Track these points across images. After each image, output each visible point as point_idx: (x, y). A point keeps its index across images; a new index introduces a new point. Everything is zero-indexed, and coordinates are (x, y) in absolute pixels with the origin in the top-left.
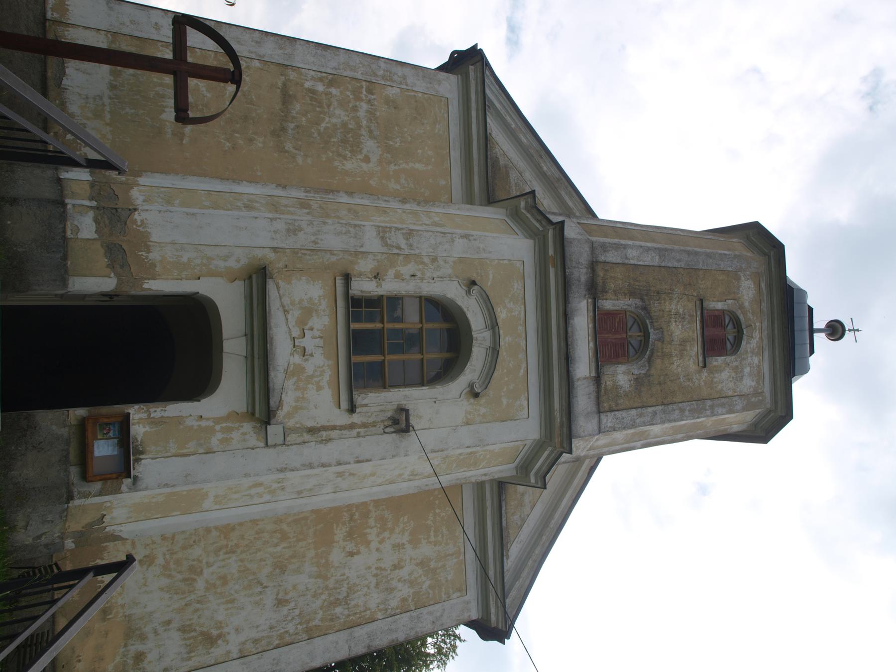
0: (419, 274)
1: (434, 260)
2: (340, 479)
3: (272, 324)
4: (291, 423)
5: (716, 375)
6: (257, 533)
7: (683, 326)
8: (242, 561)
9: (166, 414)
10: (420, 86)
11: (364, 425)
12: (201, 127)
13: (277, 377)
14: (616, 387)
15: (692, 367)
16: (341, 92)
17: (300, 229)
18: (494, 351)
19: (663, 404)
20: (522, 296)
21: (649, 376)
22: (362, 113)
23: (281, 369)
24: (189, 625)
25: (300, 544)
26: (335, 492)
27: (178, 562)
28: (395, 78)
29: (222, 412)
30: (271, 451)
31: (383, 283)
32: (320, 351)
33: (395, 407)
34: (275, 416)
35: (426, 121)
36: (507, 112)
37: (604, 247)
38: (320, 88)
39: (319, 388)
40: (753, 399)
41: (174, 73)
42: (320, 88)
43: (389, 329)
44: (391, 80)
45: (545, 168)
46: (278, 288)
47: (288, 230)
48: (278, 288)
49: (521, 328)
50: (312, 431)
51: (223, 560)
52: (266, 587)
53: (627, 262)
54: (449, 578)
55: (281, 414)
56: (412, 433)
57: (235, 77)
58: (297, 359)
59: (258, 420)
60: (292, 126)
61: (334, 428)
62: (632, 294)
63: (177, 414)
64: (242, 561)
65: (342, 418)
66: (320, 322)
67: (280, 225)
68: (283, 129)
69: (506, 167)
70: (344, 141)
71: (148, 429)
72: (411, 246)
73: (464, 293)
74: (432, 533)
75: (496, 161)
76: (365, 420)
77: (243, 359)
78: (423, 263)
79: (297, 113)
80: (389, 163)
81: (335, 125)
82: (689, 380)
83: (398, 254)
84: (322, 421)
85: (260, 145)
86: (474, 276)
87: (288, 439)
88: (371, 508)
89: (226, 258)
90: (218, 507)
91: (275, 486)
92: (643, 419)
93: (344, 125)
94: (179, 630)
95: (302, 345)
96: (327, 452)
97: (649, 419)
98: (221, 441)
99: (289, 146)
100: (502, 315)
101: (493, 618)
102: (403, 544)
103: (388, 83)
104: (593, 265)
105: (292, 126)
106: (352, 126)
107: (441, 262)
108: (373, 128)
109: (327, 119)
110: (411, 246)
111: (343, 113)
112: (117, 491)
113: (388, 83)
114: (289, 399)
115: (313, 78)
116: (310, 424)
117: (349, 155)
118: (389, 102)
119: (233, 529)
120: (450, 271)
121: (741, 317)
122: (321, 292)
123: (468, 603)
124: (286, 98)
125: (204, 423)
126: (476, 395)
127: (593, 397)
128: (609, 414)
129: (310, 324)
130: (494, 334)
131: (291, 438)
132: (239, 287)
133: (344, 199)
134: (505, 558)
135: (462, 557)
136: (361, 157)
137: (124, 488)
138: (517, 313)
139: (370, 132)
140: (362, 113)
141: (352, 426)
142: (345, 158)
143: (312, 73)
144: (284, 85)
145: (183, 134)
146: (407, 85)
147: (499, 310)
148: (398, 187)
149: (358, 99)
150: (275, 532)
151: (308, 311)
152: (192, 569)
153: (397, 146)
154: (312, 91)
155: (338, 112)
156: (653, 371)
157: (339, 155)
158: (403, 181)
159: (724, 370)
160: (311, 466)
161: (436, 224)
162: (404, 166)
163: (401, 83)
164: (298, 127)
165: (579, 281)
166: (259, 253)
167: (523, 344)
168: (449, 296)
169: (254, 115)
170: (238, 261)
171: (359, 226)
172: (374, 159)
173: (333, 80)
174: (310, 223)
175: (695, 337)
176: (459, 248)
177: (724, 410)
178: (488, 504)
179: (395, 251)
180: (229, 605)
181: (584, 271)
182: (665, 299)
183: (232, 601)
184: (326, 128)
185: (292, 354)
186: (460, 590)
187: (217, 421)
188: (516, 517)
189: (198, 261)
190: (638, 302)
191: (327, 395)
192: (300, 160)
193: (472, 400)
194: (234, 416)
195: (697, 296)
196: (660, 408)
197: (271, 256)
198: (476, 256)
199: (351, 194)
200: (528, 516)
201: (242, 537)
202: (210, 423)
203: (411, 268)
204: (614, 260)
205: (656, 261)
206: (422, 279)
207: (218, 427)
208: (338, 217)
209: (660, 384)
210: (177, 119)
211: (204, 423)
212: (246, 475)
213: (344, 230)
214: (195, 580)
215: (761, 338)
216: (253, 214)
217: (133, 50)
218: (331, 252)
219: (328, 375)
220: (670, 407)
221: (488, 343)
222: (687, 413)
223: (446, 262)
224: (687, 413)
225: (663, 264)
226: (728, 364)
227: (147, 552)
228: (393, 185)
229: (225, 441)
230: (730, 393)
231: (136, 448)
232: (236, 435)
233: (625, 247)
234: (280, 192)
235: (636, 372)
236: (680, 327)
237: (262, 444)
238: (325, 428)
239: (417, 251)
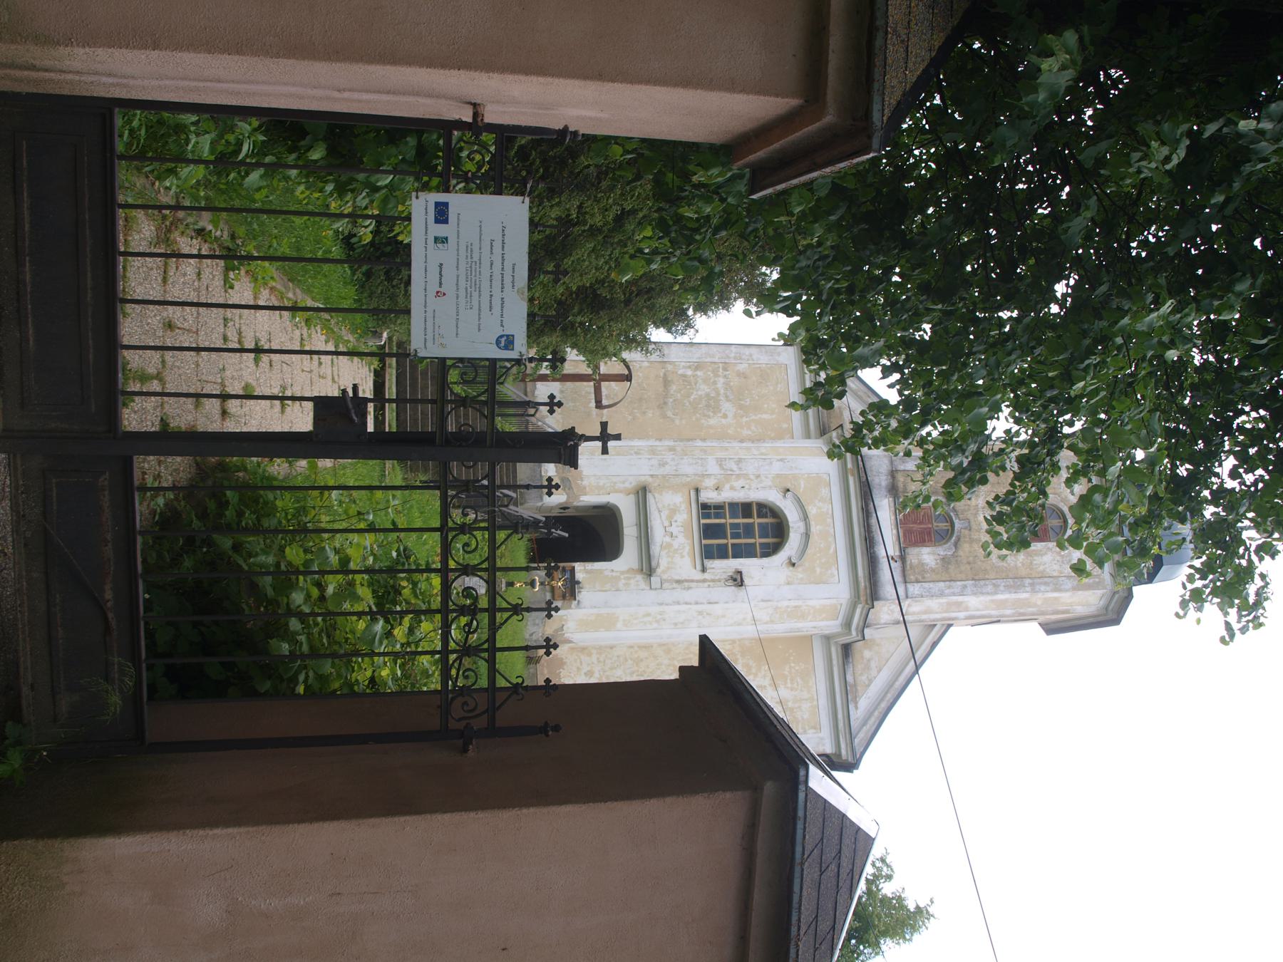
0: (747, 486)
3: (652, 519)
4: (665, 577)
5: (1035, 558)
6: (658, 665)
10: (763, 359)
11: (713, 581)
12: (613, 408)
13: (655, 549)
14: (922, 564)
17: (667, 463)
18: (807, 535)
19: (973, 579)
22: (720, 385)
23: (658, 544)
28: (743, 357)
29: (625, 568)
30: (653, 592)
31: (722, 493)
34: (655, 572)
38: (689, 373)
39: (682, 557)
42: (689, 373)
44: (741, 359)
47: (660, 464)
49: (830, 520)
50: (678, 582)
54: (805, 717)
55: (659, 571)
57: (628, 378)
58: (668, 539)
59: (645, 574)
60: (671, 400)
61: (692, 581)
63: (599, 568)
66: (682, 517)
67: (654, 462)
68: (665, 403)
70: (708, 406)
72: (740, 469)
73: (782, 497)
74: (789, 681)
76: (713, 577)
78: (749, 479)
80: (742, 417)
81: (701, 396)
84: (684, 577)
85: (651, 415)
86: (789, 486)
89: (624, 482)
91: (659, 617)
92: (952, 590)
93: (707, 395)
99: (669, 414)
100: (812, 511)
101: (844, 752)
102: (765, 686)
105: (671, 400)
107: (763, 478)
110: (740, 469)
111: (706, 387)
112: (570, 607)
115: (684, 367)
116: (677, 578)
117: (712, 414)
119: (642, 660)
122: (681, 499)
123: (822, 739)
124: (666, 382)
125: (614, 574)
126: (794, 565)
128: (915, 584)
129: (675, 518)
131: (665, 585)
132: (632, 498)
133: (699, 443)
134: (851, 706)
135: (815, 703)
136: (721, 415)
137: (573, 606)
139: (727, 397)
140: (720, 385)
141: (704, 581)
142: (709, 417)
143: (683, 364)
144: (665, 374)
145: (602, 414)
148: (750, 433)
150: (669, 665)
151: (673, 511)
153: (748, 404)
154: (684, 376)
155: (703, 387)
156: (960, 553)
157: (705, 415)
158: (753, 428)
159: (1046, 553)
160: (678, 603)
161: (762, 454)
162: (753, 417)
163: (748, 360)
164: (675, 400)
166: (643, 479)
169: (646, 396)
170: (631, 483)
171: (705, 459)
172: (730, 415)
174: (673, 459)
176: (777, 468)
177: (1048, 588)
178: (835, 662)
179: (731, 473)
181: (884, 478)
184: (695, 399)
185: (664, 536)
186: (815, 728)
187: (622, 573)
188: (864, 678)
189: (609, 485)
191: (687, 561)
192: (677, 422)
194: (631, 570)
196: (971, 582)
197: (650, 480)
199: (704, 440)
200: (875, 678)
201: (648, 667)
202: (618, 574)
203: (741, 482)
206: (749, 489)
207: (622, 577)
208: (693, 455)
209: (969, 563)
210: (597, 407)
211: (614, 574)
212: (640, 605)
213: (694, 462)
216: (640, 457)
218: (687, 476)
219: (687, 548)
220: (982, 583)
221: (802, 530)
222: (1002, 588)
223: (767, 478)
224: (1002, 588)
227: (589, 668)
228: (745, 432)
229: (626, 585)
230: (1055, 574)
232: (632, 581)
234: (658, 443)
235: (942, 553)
239: (745, 472)
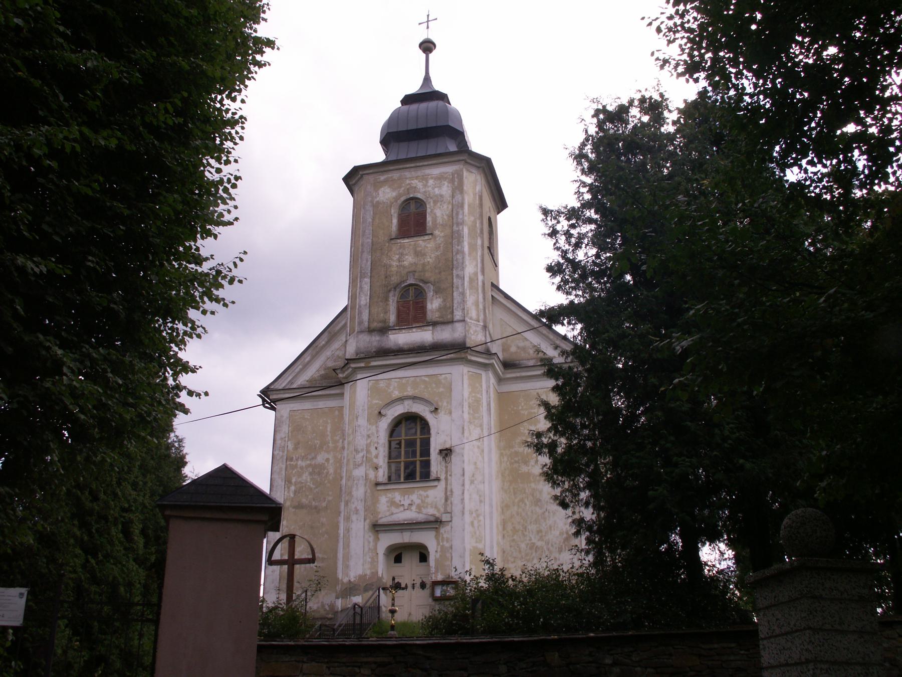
0: (376, 445)
1: (369, 436)
2: (475, 482)
4: (442, 510)
5: (438, 222)
7: (406, 255)
8: (531, 523)
9: (434, 566)
11: (446, 472)
13: (421, 517)
15: (431, 245)
16: (294, 476)
18: (414, 398)
19: (452, 270)
20: (387, 381)
21: (435, 282)
24: (559, 548)
25: (527, 491)
26: (484, 483)
27: (527, 555)
28: (283, 444)
32: (410, 496)
33: (439, 456)
35: (304, 425)
36: (293, 371)
37: (361, 323)
38: (293, 488)
39: (427, 496)
40: (456, 183)
41: (293, 565)
42: (293, 488)
43: (405, 459)
44: (284, 447)
45: (323, 343)
46: (382, 518)
47: (357, 514)
48: (382, 518)
50: (446, 499)
51: (529, 532)
52: (546, 510)
53: (368, 305)
55: (438, 515)
56: (452, 448)
58: (414, 508)
59: (439, 526)
60: (314, 503)
61: (446, 489)
62: (386, 299)
64: (531, 523)
65: (442, 484)
66: (397, 497)
68: (316, 507)
69: (325, 369)
70: (319, 474)
71: (439, 574)
72: (362, 450)
73: (385, 418)
74: (533, 411)
75: (324, 377)
76: (444, 472)
77: (412, 534)
78: (370, 443)
79: (307, 500)
80: (328, 446)
81: (311, 479)
82: (440, 247)
83: (366, 457)
84: (442, 495)
86: (377, 412)
87: (449, 511)
88: (513, 451)
89: (369, 542)
90: (483, 542)
93: (311, 474)
94: (560, 554)
95: (407, 505)
96: (457, 492)
97: (460, 281)
98: (447, 542)
99: (324, 504)
100: (396, 394)
103: (286, 448)
104: (370, 331)
105: (314, 503)
106: (310, 470)
107: (370, 432)
108: (311, 457)
109: (308, 484)
110: (362, 450)
111: (304, 475)
113: (286, 448)
114: (431, 511)
115: (288, 492)
116: (443, 501)
117: (326, 471)
118: (296, 448)
120: (374, 427)
121: (403, 199)
126: (436, 409)
127: (443, 327)
128: (455, 314)
129: (398, 502)
130: (405, 399)
132: (382, 536)
138: (396, 384)
139: (313, 458)
141: (446, 479)
142: (327, 473)
146: (285, 437)
147: (394, 396)
149: (296, 466)
151: (392, 503)
152: (531, 548)
154: (295, 492)
155: (304, 478)
156: (432, 279)
160: (463, 500)
162: (329, 438)
163: (285, 441)
164: (314, 500)
165: (379, 341)
166: (367, 527)
167: (412, 379)
168: (386, 427)
170: (371, 537)
173: (288, 481)
175: (413, 243)
177: (461, 212)
179: (365, 459)
180: (553, 528)
182: (390, 271)
183: (550, 527)
184: (313, 484)
185: (411, 510)
187: (438, 544)
189: (370, 554)
190: (391, 294)
191: (431, 493)
192: (330, 498)
193: (439, 411)
194: (437, 537)
195: (388, 242)
196: (454, 271)
197: (368, 521)
198: (366, 412)
200: (531, 343)
201: (519, 523)
202: (439, 547)
203: (373, 449)
204: (367, 315)
205: (367, 280)
206: (378, 443)
207: (441, 544)
209: (440, 273)
211: (439, 550)
214: (537, 547)
215: (417, 178)
217: (285, 581)
218: (366, 492)
221: (410, 402)
222: (459, 248)
224: (459, 248)
225: (369, 274)
226: (431, 212)
230: (450, 207)
231: (447, 578)
232: (445, 536)
233: (360, 306)
234: (342, 515)
235: (432, 293)
236: (407, 257)
237: (450, 523)
238: (446, 493)
239: (365, 446)
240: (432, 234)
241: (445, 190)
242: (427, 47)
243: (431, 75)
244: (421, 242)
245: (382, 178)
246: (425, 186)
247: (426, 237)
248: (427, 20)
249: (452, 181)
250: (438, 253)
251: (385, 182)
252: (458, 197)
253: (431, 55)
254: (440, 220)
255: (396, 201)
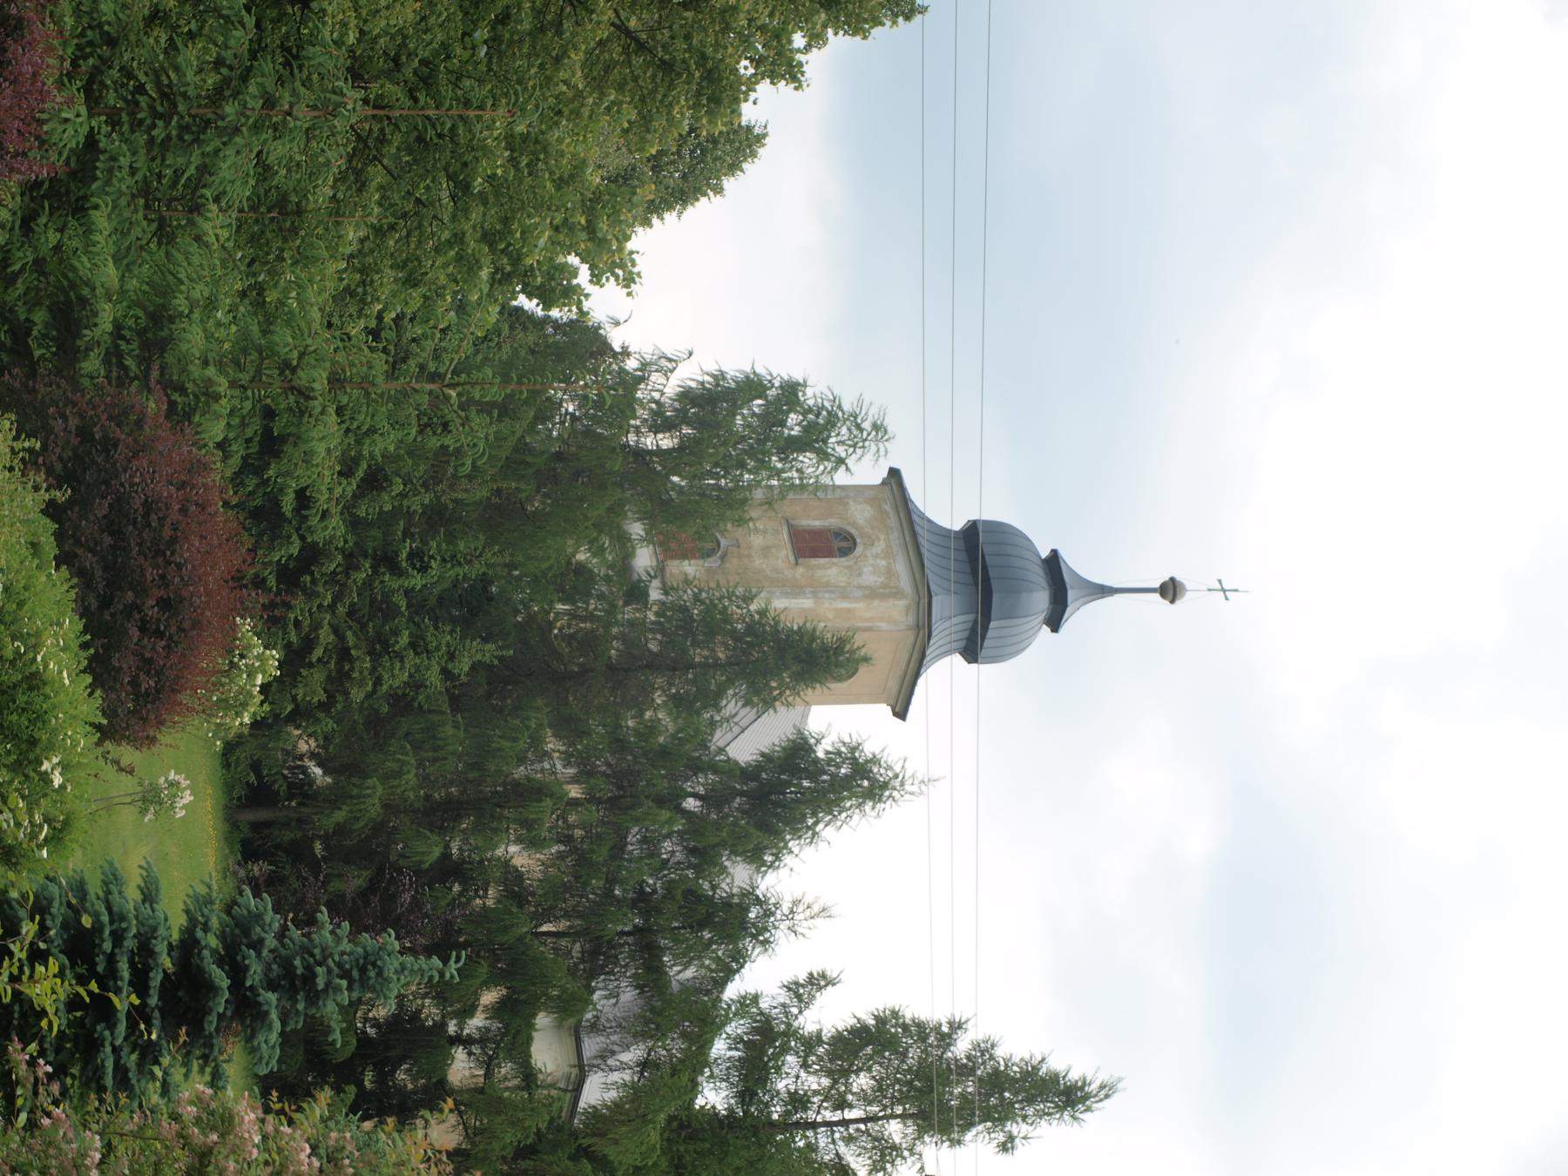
15: (780, 563)
121: (853, 531)
156: (727, 565)
240: (797, 564)
241: (869, 577)
242: (1170, 590)
243: (1117, 597)
244: (784, 552)
245: (888, 507)
246: (876, 556)
247: (792, 558)
248: (1226, 587)
249: (885, 586)
250: (768, 572)
251: (881, 511)
252: (859, 593)
253: (1157, 596)
254: (819, 573)
255: (849, 524)
